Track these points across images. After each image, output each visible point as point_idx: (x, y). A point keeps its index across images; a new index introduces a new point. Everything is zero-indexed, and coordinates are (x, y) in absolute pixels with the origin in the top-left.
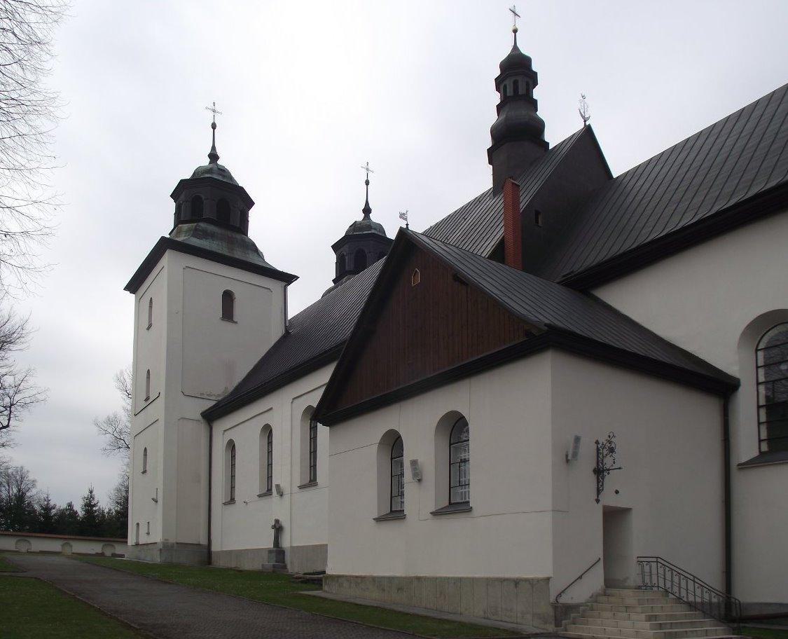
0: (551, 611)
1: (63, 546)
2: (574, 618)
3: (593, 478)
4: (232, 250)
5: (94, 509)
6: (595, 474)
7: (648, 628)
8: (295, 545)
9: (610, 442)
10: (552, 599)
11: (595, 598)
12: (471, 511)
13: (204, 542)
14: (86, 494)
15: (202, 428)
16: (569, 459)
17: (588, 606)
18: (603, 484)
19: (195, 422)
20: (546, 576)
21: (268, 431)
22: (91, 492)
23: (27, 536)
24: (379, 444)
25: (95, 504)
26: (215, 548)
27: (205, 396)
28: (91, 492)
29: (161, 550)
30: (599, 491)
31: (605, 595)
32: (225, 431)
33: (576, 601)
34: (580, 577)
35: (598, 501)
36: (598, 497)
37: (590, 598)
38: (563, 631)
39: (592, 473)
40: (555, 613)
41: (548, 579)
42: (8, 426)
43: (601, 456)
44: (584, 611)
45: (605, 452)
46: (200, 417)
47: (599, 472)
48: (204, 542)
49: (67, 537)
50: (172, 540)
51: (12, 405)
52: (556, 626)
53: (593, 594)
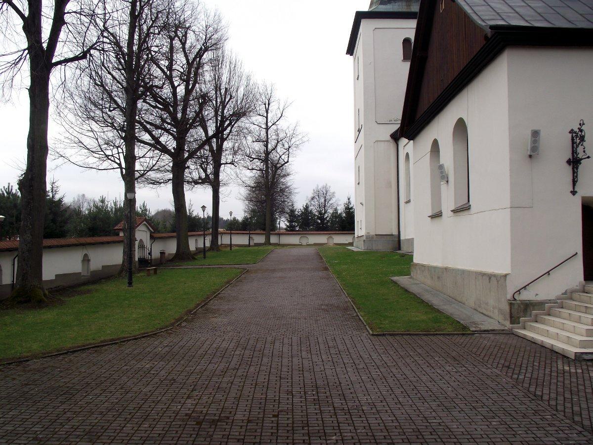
0: (506, 308)
1: (328, 239)
2: (536, 315)
3: (568, 169)
4: (409, 6)
5: (351, 210)
6: (570, 164)
7: (585, 334)
8: (406, 238)
9: (581, 131)
10: (509, 296)
11: (569, 295)
12: (469, 209)
13: (395, 233)
14: (346, 201)
15: (392, 145)
16: (533, 153)
17: (557, 303)
18: (577, 174)
19: (386, 142)
20: (505, 272)
21: (435, 144)
22: (349, 199)
23: (305, 234)
24: (431, 151)
25: (352, 207)
26: (402, 238)
27: (393, 122)
28: (349, 199)
29: (364, 241)
30: (574, 182)
31: (584, 291)
32: (404, 146)
33: (542, 297)
34: (548, 273)
35: (574, 193)
36: (574, 188)
37: (563, 294)
38: (521, 329)
39: (567, 164)
40: (511, 310)
41: (506, 276)
42: (288, 162)
43: (575, 145)
44: (550, 308)
45: (578, 141)
46: (389, 138)
47: (574, 162)
48: (395, 233)
49: (330, 232)
50: (372, 233)
51: (289, 147)
52: (511, 323)
53: (566, 291)
